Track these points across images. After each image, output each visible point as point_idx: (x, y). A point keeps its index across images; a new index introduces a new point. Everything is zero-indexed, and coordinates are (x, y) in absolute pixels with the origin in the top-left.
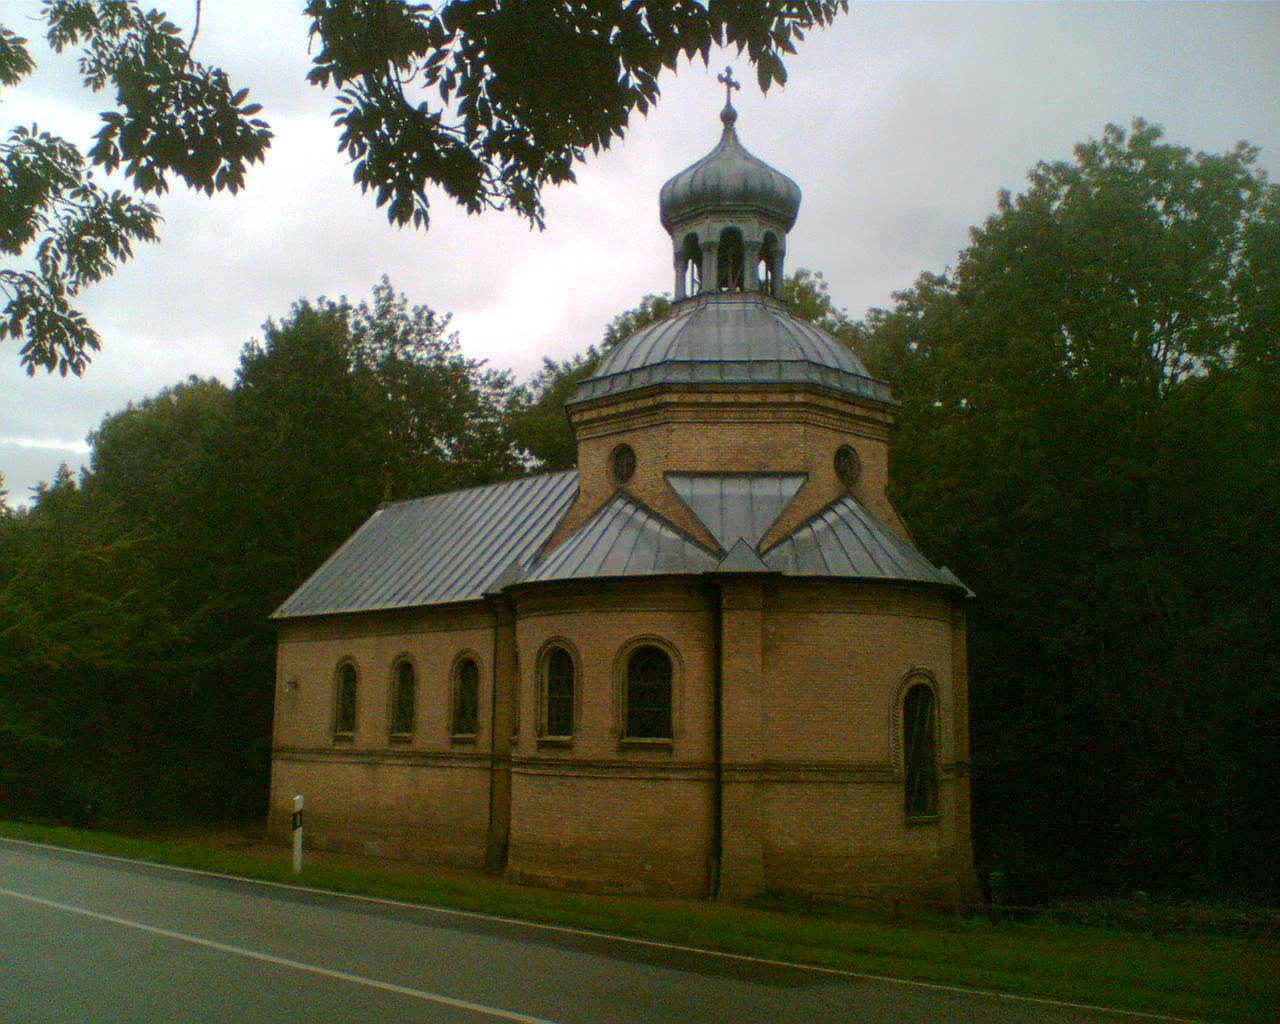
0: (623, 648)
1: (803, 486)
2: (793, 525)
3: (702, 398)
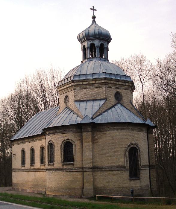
0: (63, 142)
1: (105, 101)
2: (103, 111)
3: (81, 83)
